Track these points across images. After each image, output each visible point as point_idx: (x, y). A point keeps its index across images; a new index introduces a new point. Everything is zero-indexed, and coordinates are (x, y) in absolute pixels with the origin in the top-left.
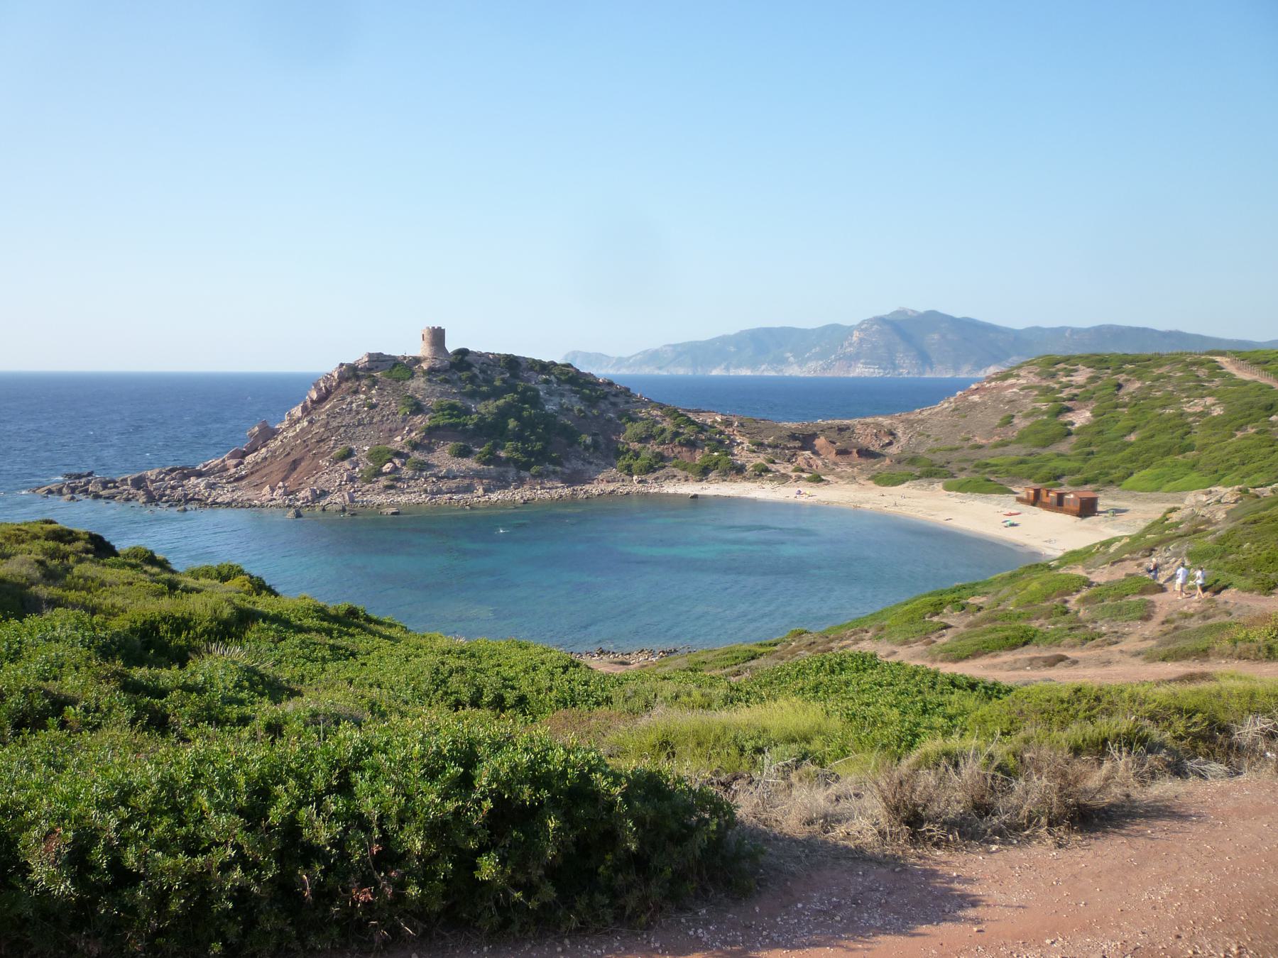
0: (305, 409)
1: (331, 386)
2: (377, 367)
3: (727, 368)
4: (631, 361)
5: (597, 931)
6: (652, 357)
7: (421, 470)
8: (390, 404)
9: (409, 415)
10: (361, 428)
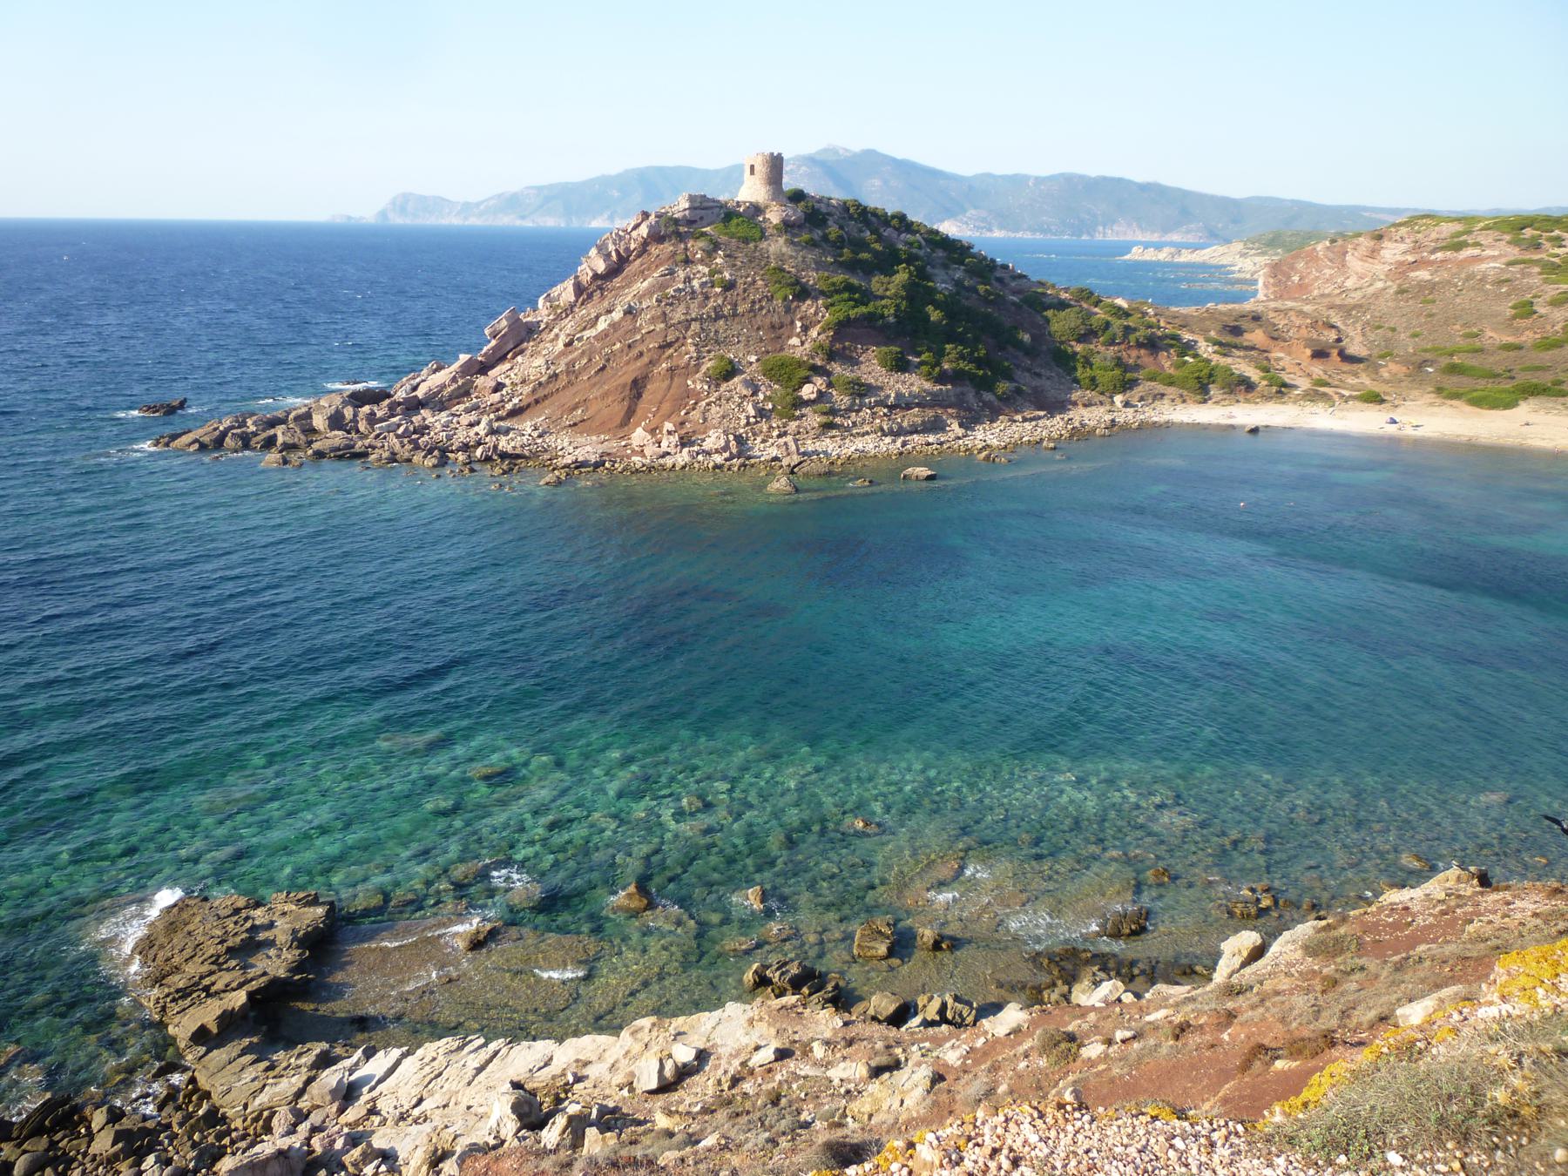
0: (579, 289)
1: (627, 249)
2: (701, 218)
3: (611, 218)
4: (482, 207)
5: (564, 1074)
6: (512, 202)
7: (861, 396)
8: (754, 282)
9: (792, 301)
10: (721, 322)
